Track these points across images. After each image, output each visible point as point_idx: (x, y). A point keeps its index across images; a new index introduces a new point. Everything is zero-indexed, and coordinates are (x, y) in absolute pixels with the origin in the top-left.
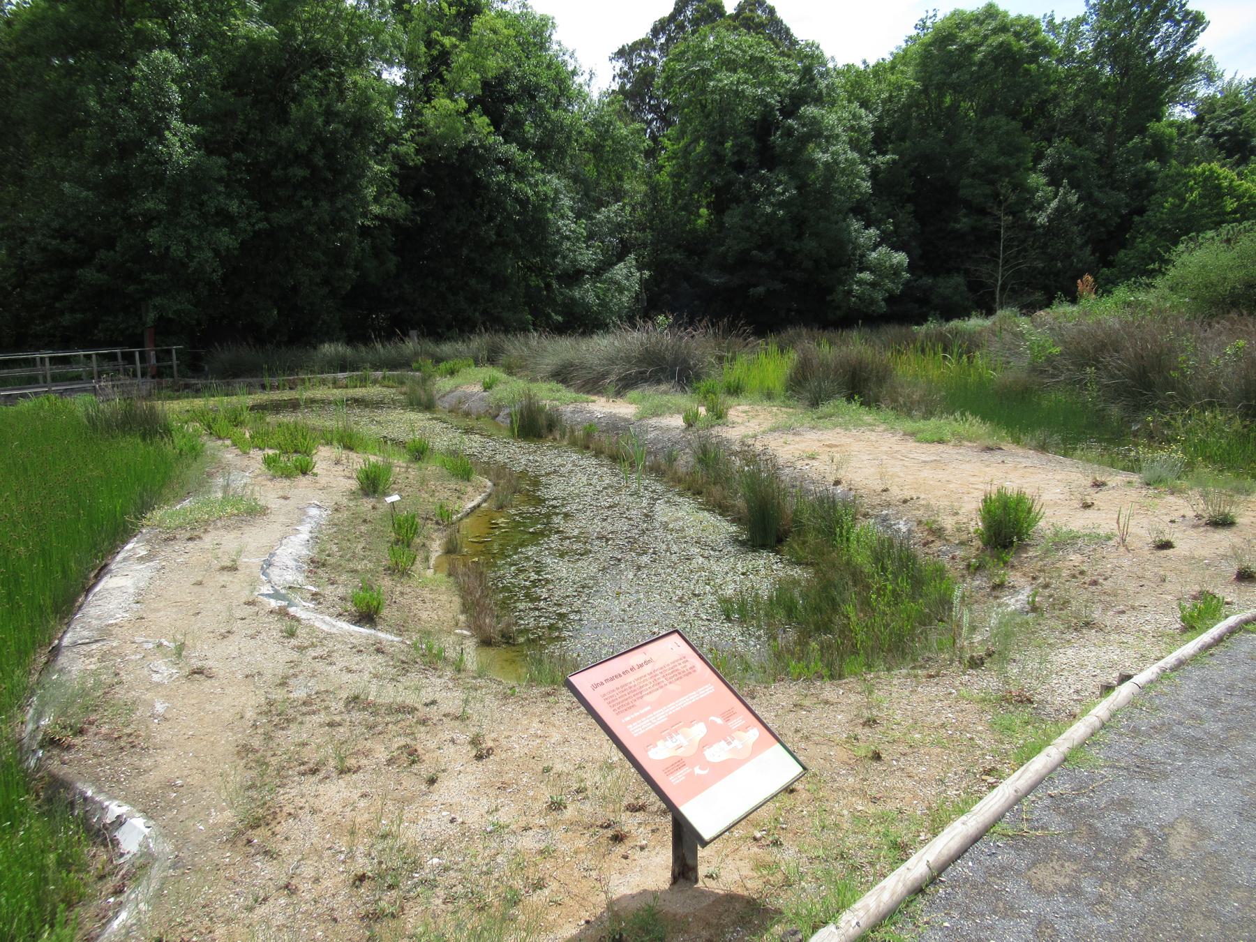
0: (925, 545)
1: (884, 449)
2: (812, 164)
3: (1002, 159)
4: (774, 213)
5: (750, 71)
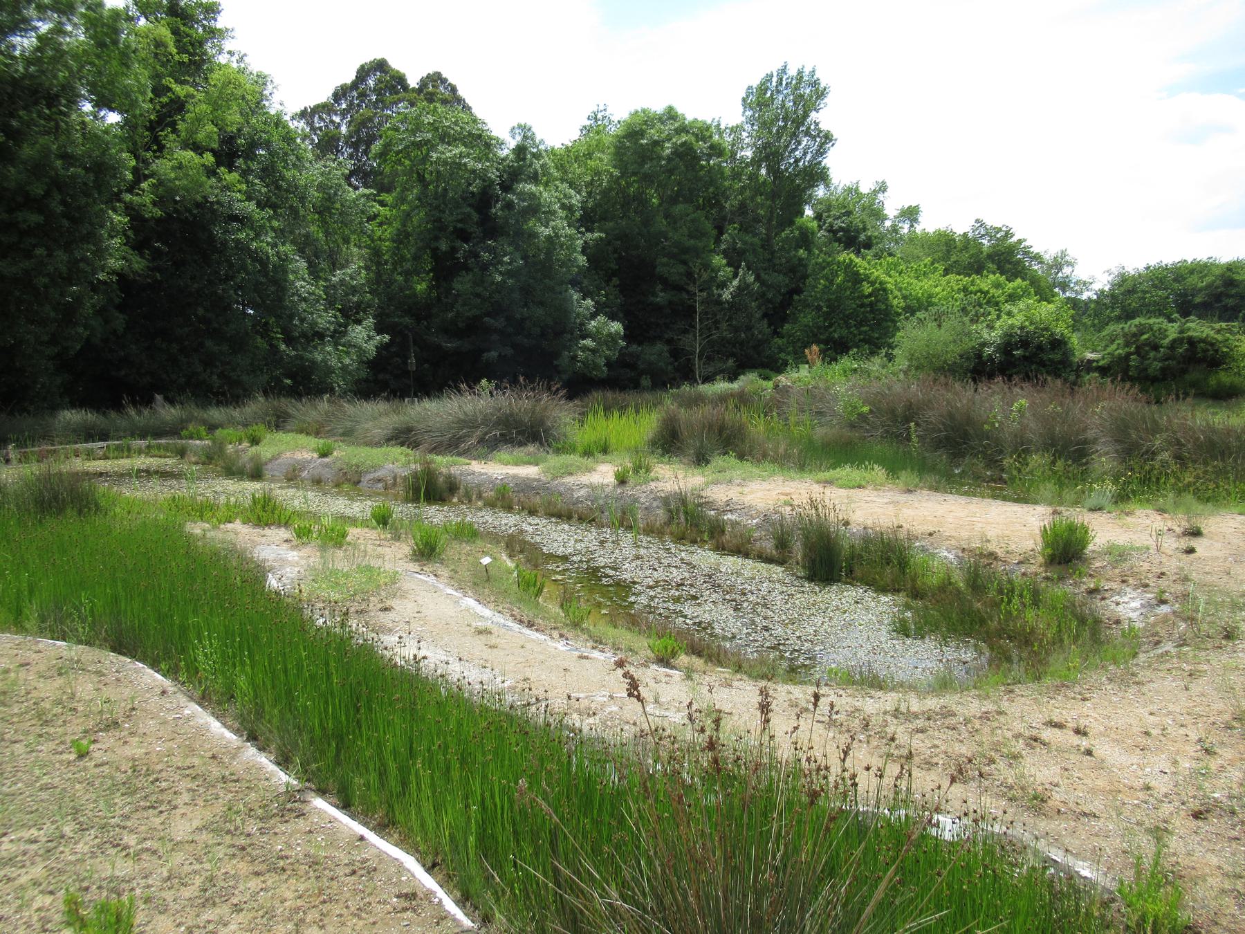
2: (533, 235)
4: (504, 281)
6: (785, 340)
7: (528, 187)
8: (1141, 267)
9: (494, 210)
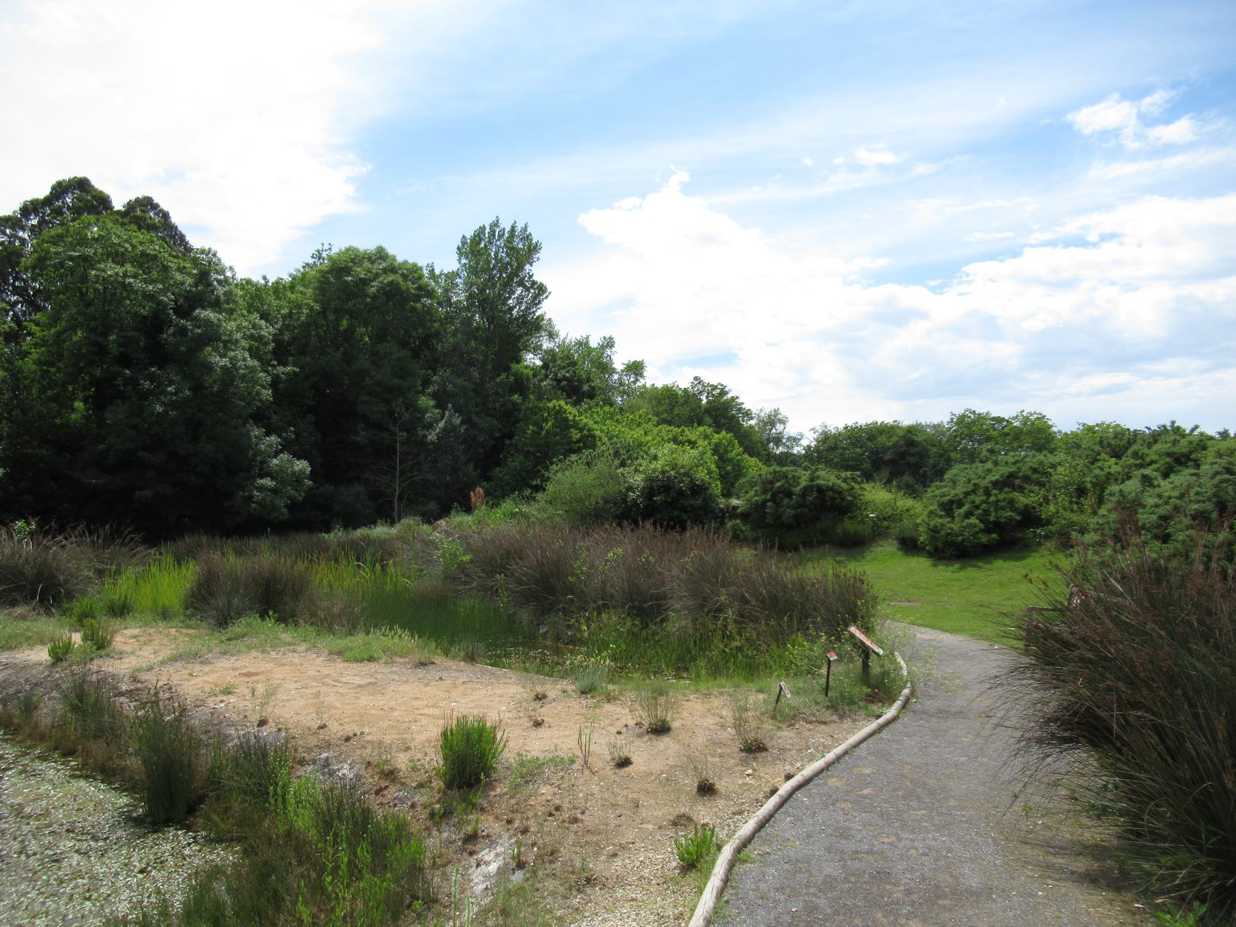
0: (377, 793)
1: (312, 673)
2: (209, 368)
3: (396, 381)
4: (165, 413)
5: (141, 266)
6: (493, 484)
7: (206, 313)
8: (841, 427)
9: (165, 336)
